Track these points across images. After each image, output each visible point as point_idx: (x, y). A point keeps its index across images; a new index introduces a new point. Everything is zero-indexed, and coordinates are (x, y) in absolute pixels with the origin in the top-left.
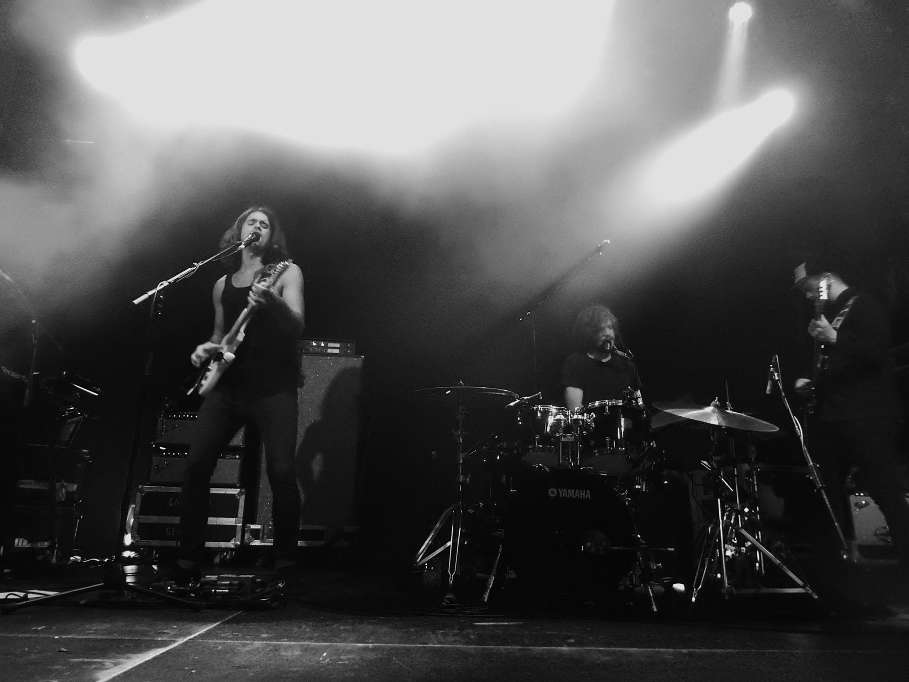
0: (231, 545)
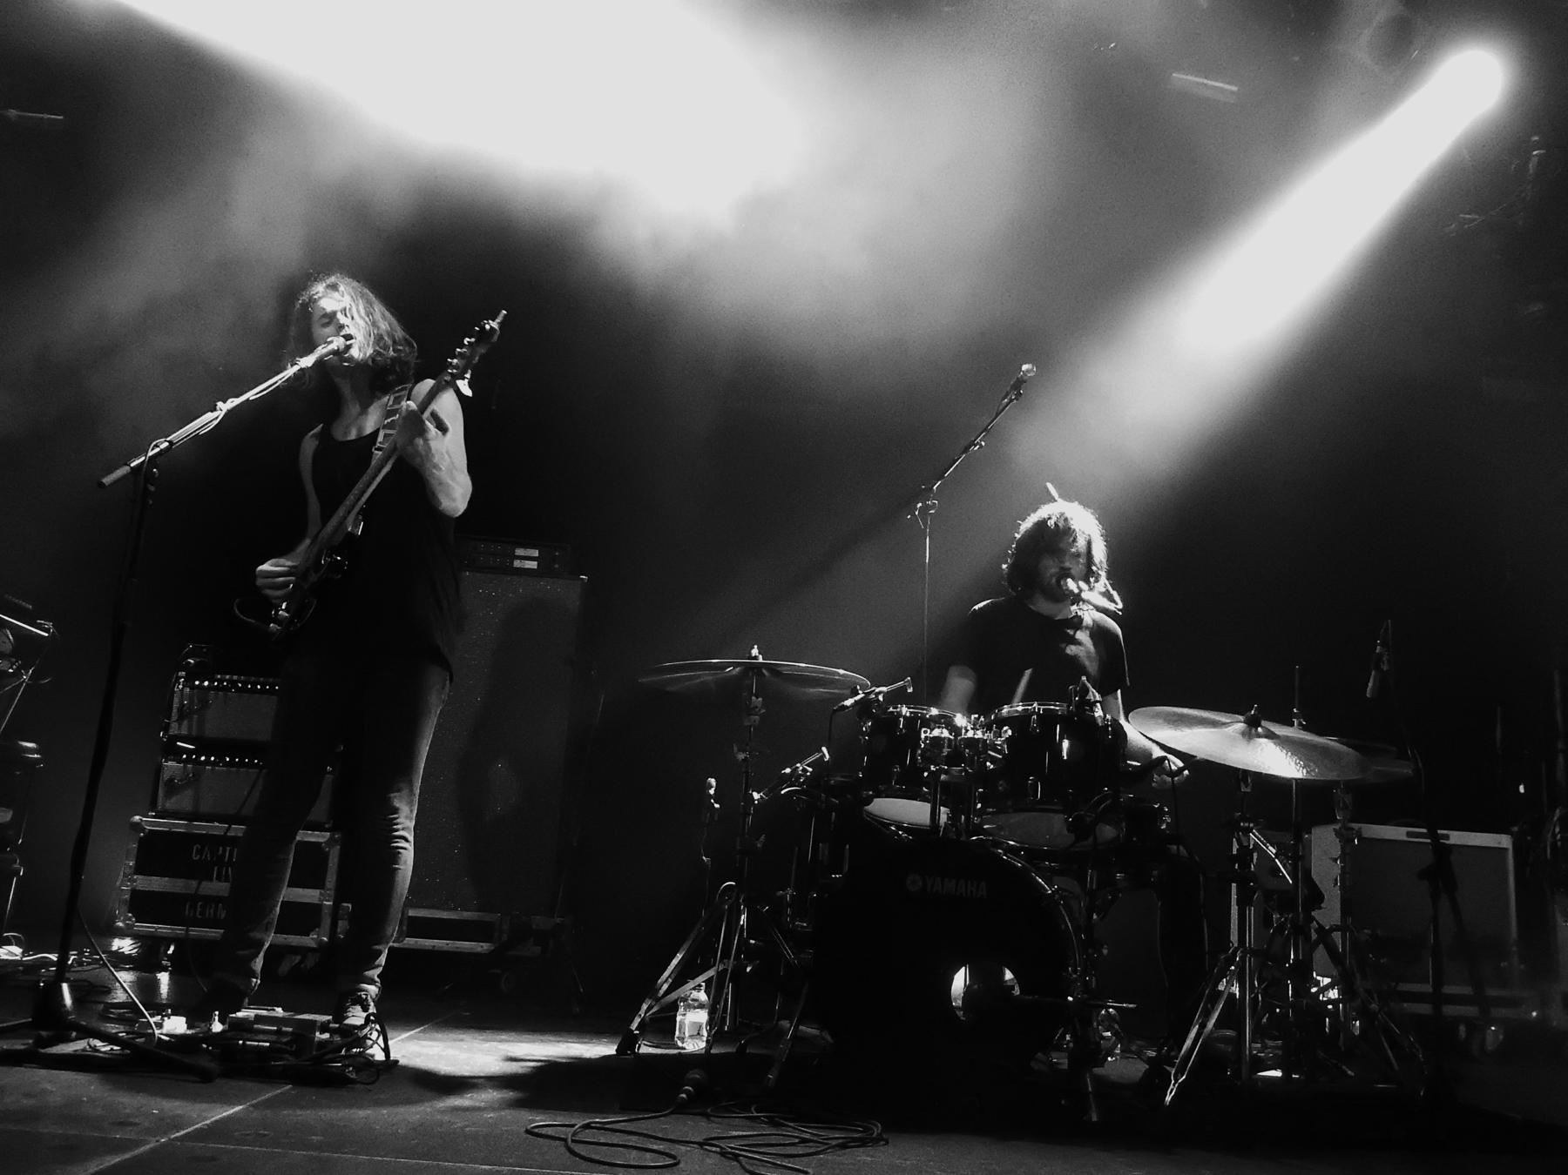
0: (310, 940)
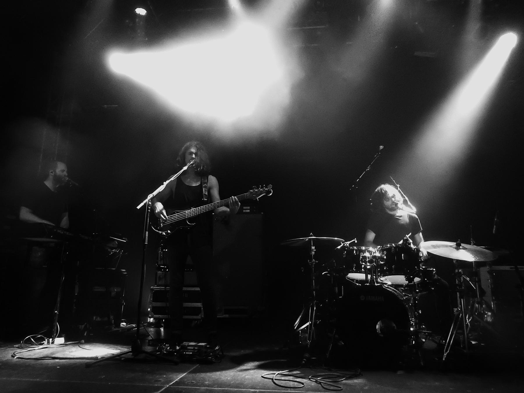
0: (199, 317)
